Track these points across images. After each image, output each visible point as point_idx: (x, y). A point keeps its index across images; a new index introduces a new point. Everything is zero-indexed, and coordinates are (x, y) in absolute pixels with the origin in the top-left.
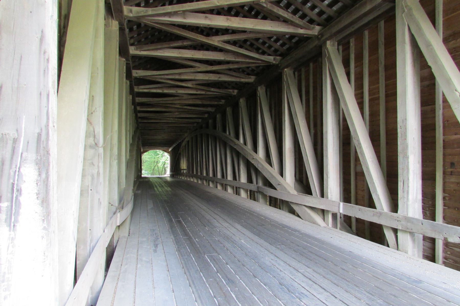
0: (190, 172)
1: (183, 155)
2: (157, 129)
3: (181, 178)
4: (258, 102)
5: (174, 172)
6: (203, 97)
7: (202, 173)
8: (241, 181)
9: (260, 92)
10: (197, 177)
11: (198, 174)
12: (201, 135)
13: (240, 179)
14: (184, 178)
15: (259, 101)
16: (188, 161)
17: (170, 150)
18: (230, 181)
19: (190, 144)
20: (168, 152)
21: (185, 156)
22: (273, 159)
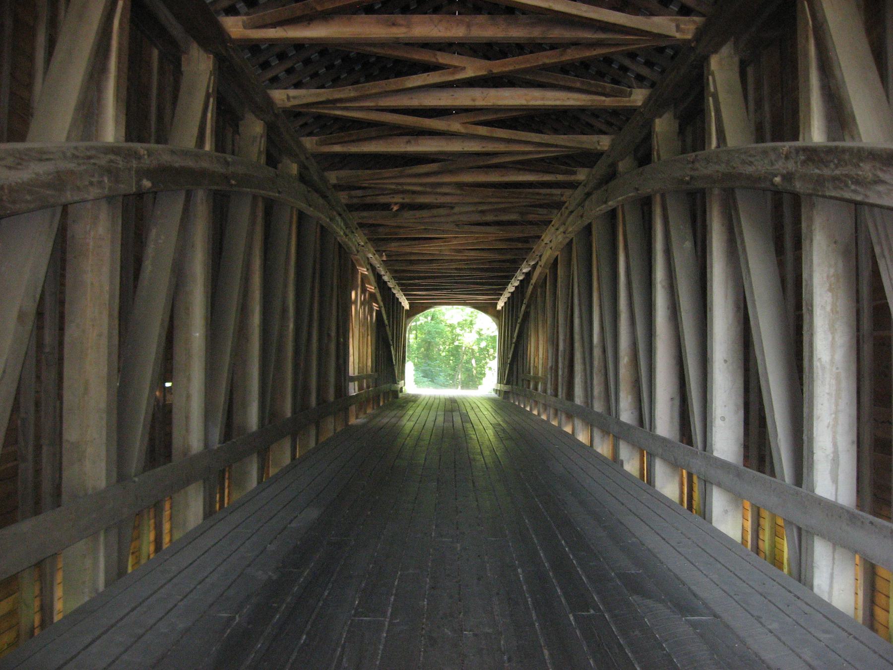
0: (560, 393)
1: (536, 319)
2: (122, 619)
3: (528, 409)
4: (710, 116)
5: (508, 383)
6: (370, 360)
7: (613, 409)
8: (654, 432)
9: (717, 78)
10: (591, 420)
11: (592, 407)
12: (645, 205)
13: (708, 434)
14: (539, 414)
15: (713, 114)
16: (554, 342)
17: (500, 305)
18: (663, 440)
19: (560, 272)
20: (496, 315)
21: (543, 326)
22: (763, 336)
